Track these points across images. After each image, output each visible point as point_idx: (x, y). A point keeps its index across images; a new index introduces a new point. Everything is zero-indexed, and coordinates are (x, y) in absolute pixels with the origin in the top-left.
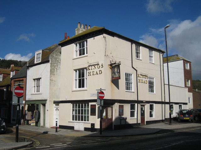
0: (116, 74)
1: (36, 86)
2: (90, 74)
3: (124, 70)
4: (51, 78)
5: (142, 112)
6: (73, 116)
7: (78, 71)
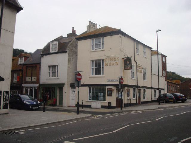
2: (107, 65)
7: (94, 62)
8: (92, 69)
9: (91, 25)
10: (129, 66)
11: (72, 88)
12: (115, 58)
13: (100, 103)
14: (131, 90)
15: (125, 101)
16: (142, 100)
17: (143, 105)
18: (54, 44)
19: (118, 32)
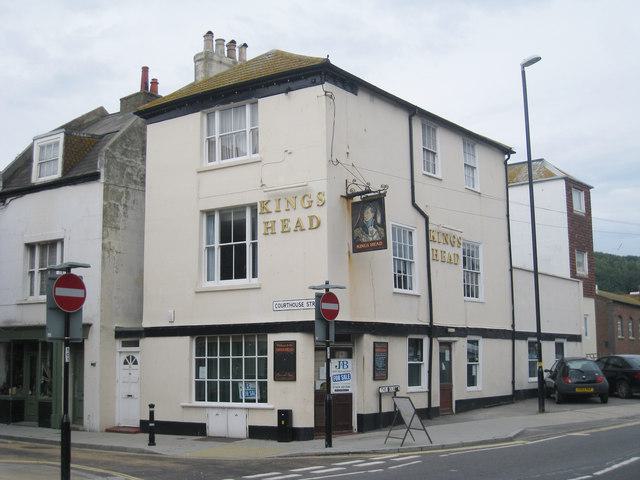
0: (371, 229)
1: (37, 269)
3: (398, 212)
4: (106, 241)
5: (444, 368)
6: (199, 386)
8: (210, 250)
9: (213, 49)
10: (374, 234)
11: (125, 344)
12: (305, 197)
13: (244, 412)
14: (399, 350)
15: (364, 403)
16: (461, 391)
17: (462, 416)
18: (49, 146)
19: (322, 72)
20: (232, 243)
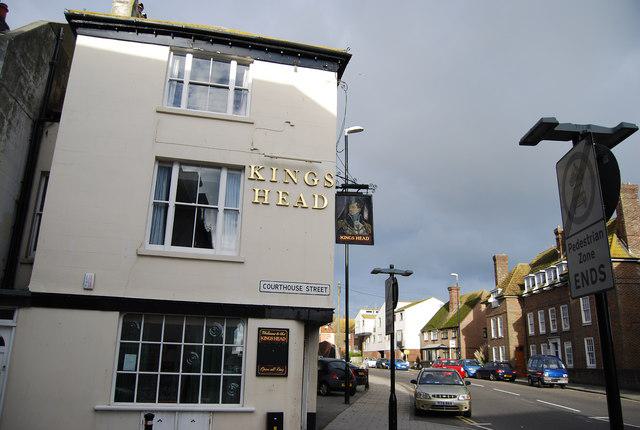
0: (357, 223)
13: (207, 417)
20: (197, 205)
